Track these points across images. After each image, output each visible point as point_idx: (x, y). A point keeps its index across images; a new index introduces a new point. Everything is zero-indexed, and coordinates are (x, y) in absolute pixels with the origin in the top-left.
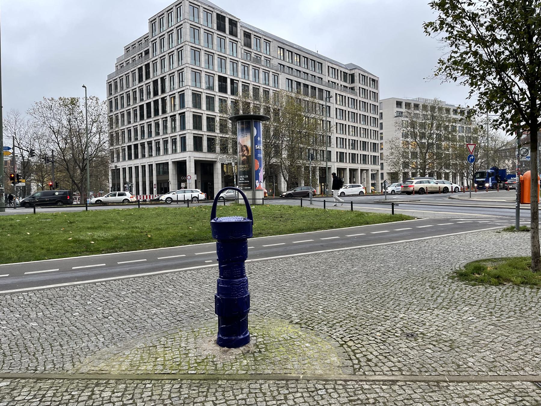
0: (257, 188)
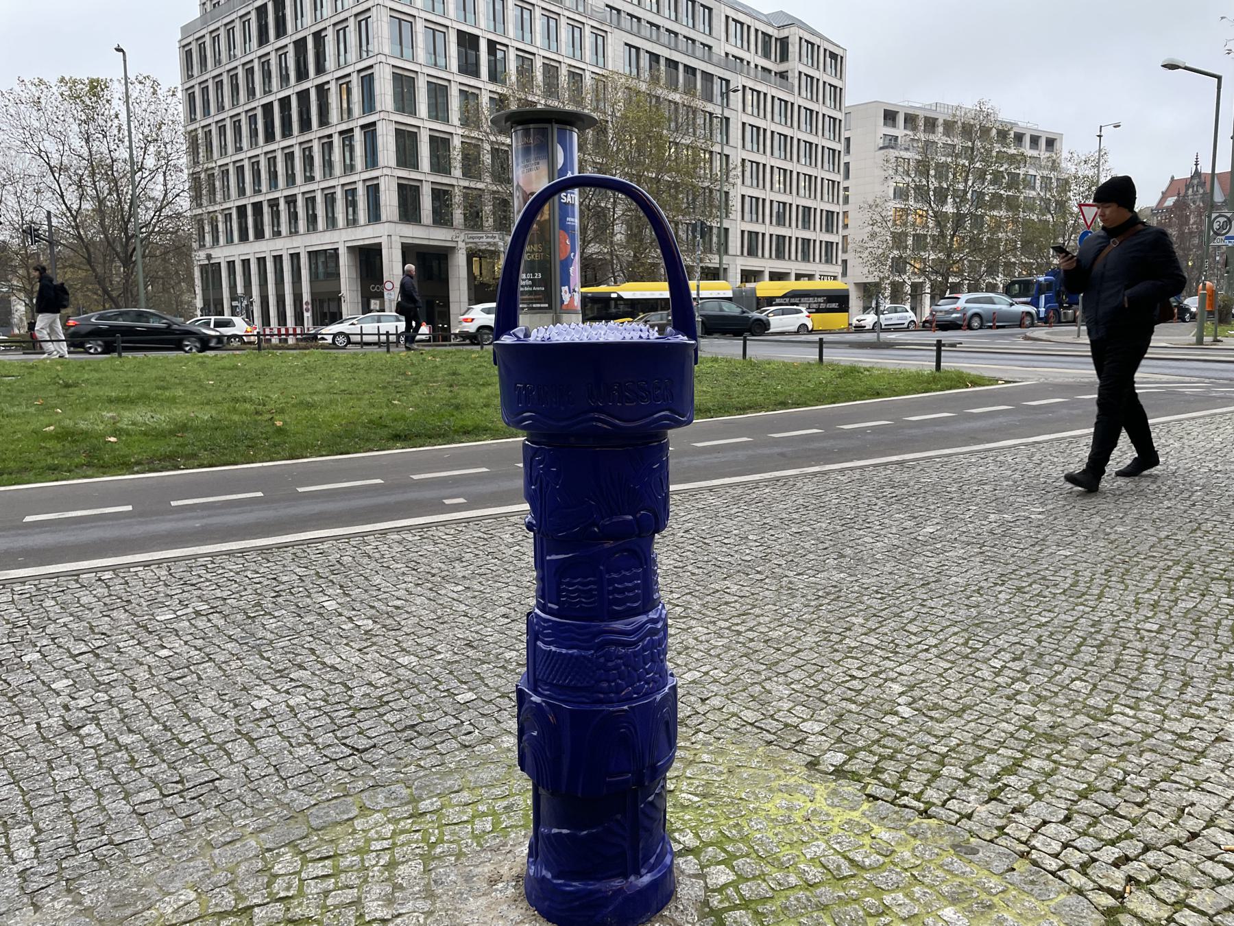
0: (564, 307)
